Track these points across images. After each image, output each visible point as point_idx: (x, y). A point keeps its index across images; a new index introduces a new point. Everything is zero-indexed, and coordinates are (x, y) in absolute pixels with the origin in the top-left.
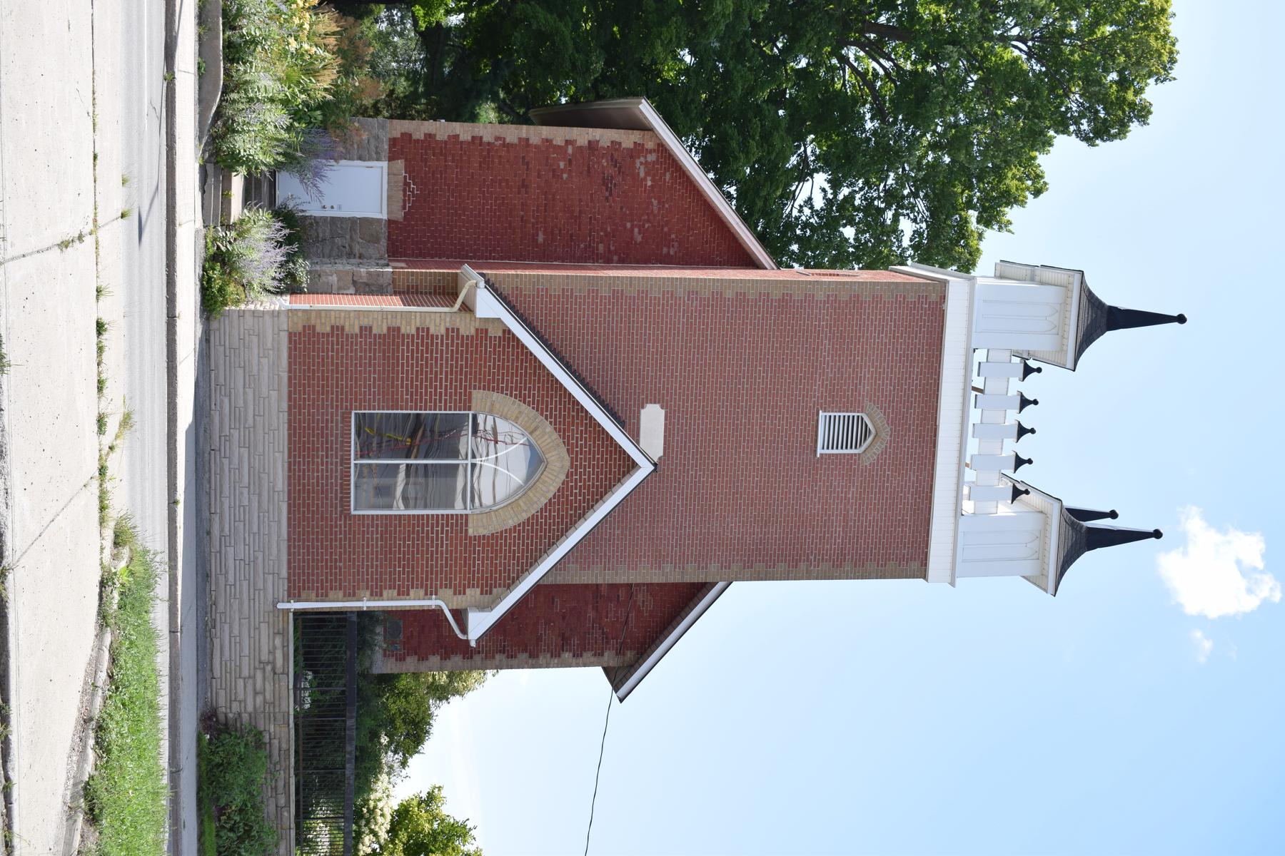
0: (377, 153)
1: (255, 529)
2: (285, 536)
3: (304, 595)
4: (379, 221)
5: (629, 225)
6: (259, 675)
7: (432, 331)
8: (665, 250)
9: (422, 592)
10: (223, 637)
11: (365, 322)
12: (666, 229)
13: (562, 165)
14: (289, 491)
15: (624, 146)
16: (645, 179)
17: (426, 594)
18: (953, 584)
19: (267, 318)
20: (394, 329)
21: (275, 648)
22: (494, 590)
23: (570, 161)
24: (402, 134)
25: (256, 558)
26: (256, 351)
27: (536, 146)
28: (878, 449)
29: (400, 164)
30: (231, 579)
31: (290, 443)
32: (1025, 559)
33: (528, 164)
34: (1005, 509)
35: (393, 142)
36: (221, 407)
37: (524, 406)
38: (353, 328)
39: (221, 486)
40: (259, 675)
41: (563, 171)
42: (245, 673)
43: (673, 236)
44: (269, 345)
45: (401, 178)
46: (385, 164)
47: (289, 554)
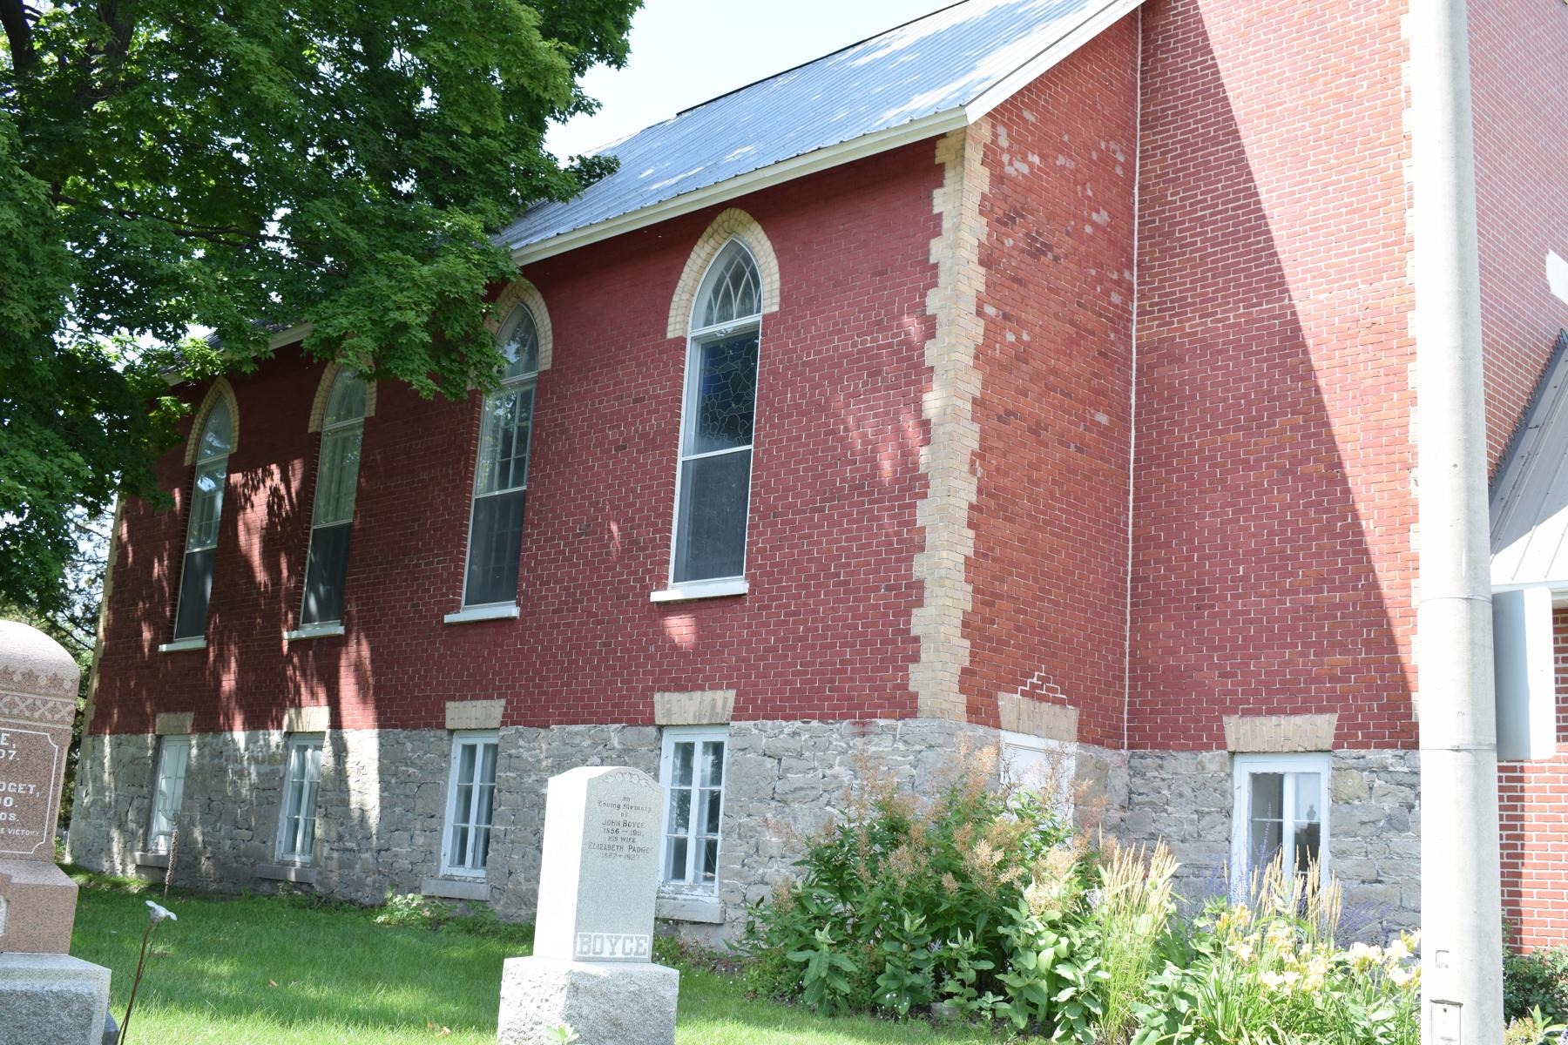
12: (1094, 156)
16: (1031, 165)
24: (961, 691)
27: (985, 385)
29: (1008, 702)
33: (1009, 413)
41: (1019, 338)
45: (1026, 703)
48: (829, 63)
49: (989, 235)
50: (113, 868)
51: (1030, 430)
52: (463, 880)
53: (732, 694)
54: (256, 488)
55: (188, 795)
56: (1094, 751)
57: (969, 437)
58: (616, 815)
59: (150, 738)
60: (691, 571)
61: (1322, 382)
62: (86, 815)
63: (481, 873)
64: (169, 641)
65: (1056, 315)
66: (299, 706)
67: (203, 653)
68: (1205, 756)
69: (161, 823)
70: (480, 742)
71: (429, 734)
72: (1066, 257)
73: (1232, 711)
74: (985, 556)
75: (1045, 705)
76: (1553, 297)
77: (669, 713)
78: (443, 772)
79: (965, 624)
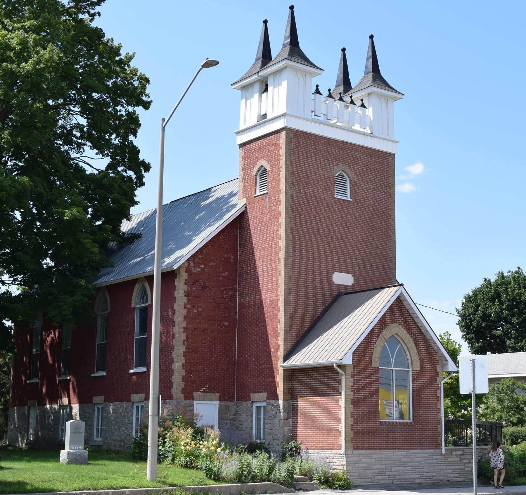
0: (191, 406)
1: (418, 464)
2: (421, 450)
3: (440, 442)
4: (220, 405)
5: (221, 278)
6: (464, 461)
7: (352, 384)
8: (232, 260)
9: (438, 391)
10: (453, 477)
11: (349, 415)
12: (223, 259)
13: (195, 311)
14: (407, 449)
15: (187, 278)
16: (201, 268)
17: (438, 389)
18: (397, 142)
19: (349, 460)
20: (352, 402)
21: (456, 455)
22: (437, 359)
23: (194, 307)
24: (182, 393)
25: (428, 463)
26: (360, 465)
27: (187, 324)
28: (348, 171)
29: (195, 394)
30: (434, 474)
31: (390, 449)
32: (305, 81)
33: (195, 329)
34: (369, 112)
35: (186, 398)
36: (378, 480)
37: (377, 343)
38: (351, 421)
39: (405, 479)
40: (464, 461)
41: (198, 311)
42: (463, 467)
43: (226, 256)
44: (358, 458)
45: (202, 394)
46: (195, 402)
47: (426, 449)
48: (202, 193)
49: (188, 289)
50: (19, 445)
51: (202, 331)
52: (98, 441)
53: (144, 394)
54: (48, 337)
55: (37, 423)
56: (224, 403)
57: (183, 337)
58: (76, 428)
59: (26, 408)
60: (137, 366)
61: (266, 316)
62: (12, 430)
63: (101, 439)
64: (29, 380)
65: (210, 302)
66: (61, 398)
67: (38, 382)
68: (248, 402)
69: (31, 431)
70: (100, 407)
71: (90, 405)
72: (213, 287)
73: (251, 392)
74: (188, 363)
75: (208, 394)
76: (336, 284)
77: (134, 399)
78: (93, 414)
79: (183, 379)
